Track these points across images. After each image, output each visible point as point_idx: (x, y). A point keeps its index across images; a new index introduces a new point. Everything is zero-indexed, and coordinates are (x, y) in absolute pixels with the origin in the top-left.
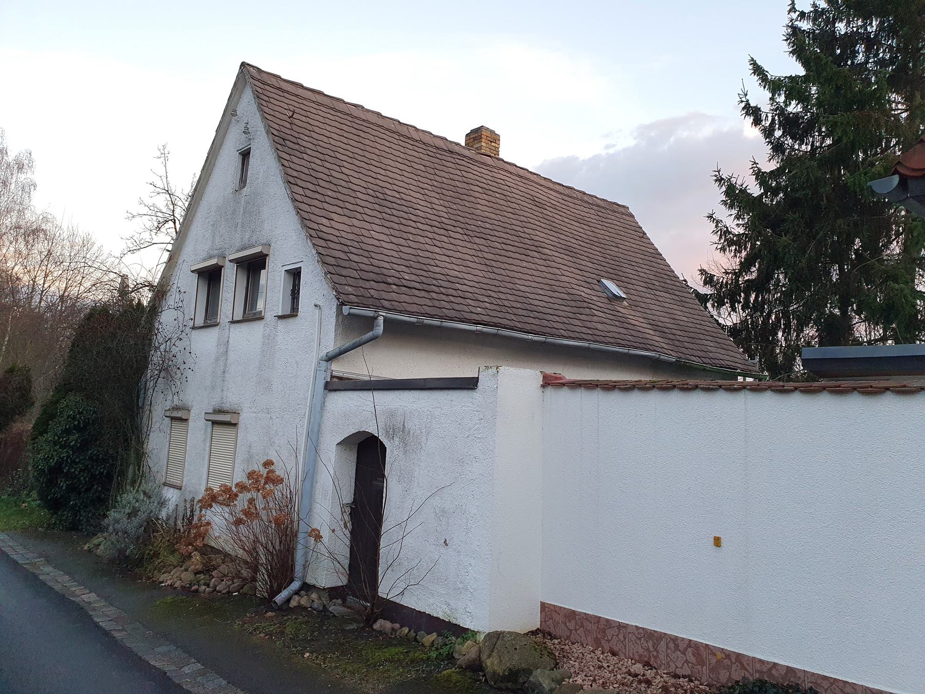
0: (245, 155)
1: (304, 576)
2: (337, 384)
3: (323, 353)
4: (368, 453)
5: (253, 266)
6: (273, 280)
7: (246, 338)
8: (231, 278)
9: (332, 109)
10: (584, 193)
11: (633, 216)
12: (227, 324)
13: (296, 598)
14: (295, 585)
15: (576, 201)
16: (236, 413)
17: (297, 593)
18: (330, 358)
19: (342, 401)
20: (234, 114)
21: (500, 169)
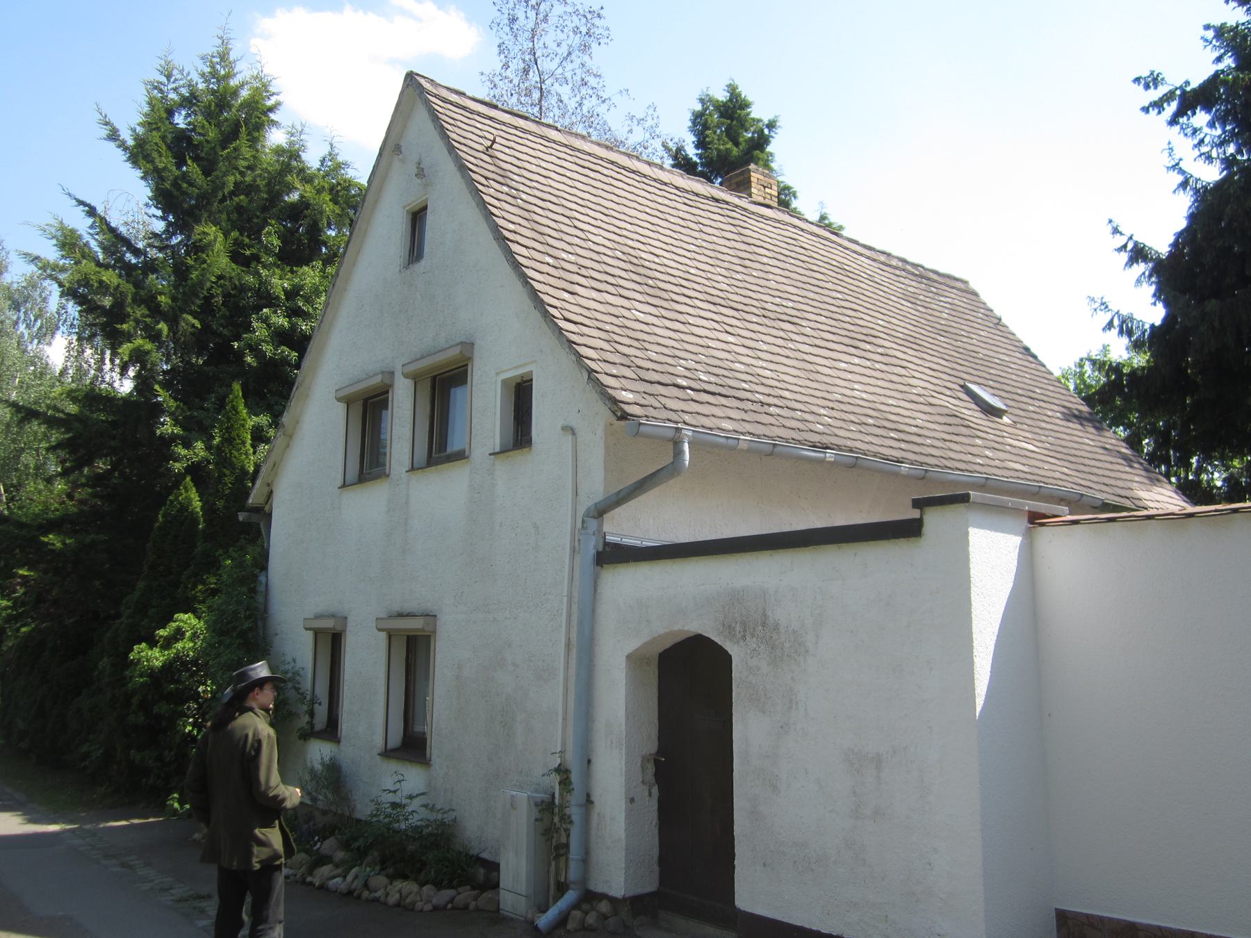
0: (417, 218)
1: (584, 880)
2: (614, 555)
3: (586, 503)
4: (692, 683)
5: (444, 382)
6: (483, 411)
7: (443, 493)
8: (403, 400)
9: (566, 146)
10: (889, 255)
11: (976, 294)
12: (404, 475)
13: (577, 914)
14: (570, 896)
15: (898, 272)
16: (431, 616)
17: (576, 906)
18: (600, 511)
19: (625, 584)
20: (398, 149)
21: (787, 224)
